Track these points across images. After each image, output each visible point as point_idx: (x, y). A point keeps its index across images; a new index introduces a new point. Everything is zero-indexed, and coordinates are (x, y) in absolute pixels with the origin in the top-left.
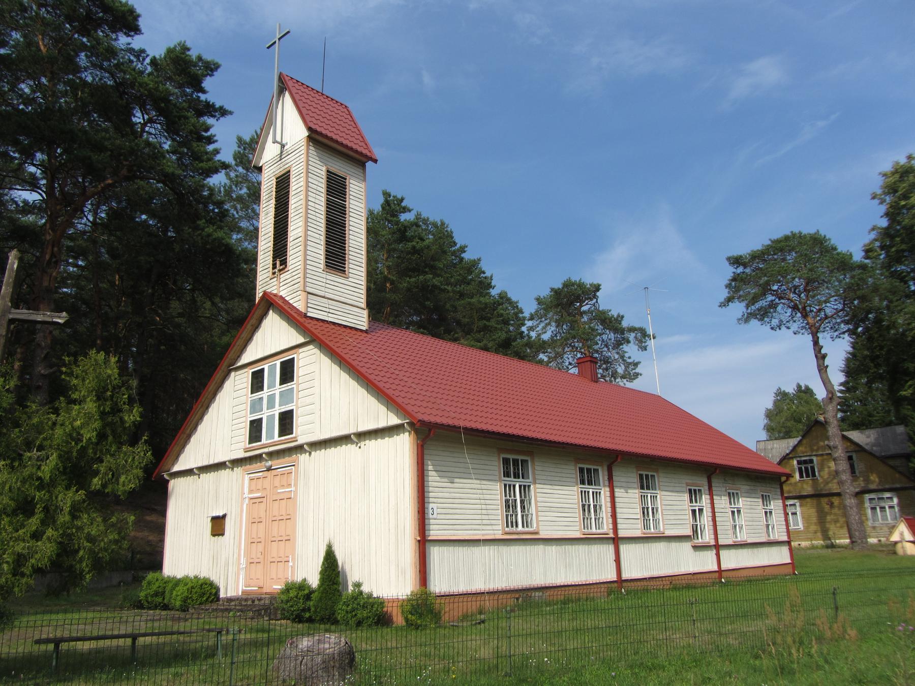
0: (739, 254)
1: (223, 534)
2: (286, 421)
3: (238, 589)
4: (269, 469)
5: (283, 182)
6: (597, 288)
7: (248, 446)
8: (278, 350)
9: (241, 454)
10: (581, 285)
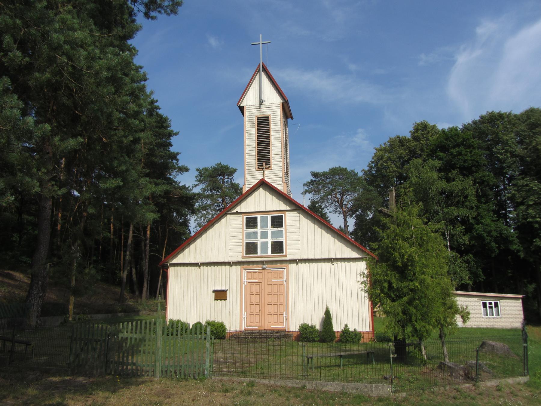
0: (318, 171)
1: (225, 299)
2: (278, 247)
3: (241, 326)
4: (263, 269)
5: (263, 123)
6: (235, 171)
7: (245, 255)
8: (261, 210)
9: (240, 259)
10: (227, 167)
